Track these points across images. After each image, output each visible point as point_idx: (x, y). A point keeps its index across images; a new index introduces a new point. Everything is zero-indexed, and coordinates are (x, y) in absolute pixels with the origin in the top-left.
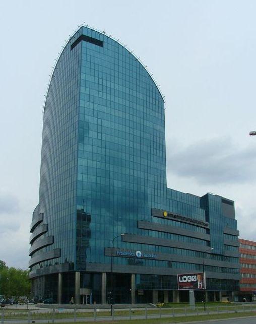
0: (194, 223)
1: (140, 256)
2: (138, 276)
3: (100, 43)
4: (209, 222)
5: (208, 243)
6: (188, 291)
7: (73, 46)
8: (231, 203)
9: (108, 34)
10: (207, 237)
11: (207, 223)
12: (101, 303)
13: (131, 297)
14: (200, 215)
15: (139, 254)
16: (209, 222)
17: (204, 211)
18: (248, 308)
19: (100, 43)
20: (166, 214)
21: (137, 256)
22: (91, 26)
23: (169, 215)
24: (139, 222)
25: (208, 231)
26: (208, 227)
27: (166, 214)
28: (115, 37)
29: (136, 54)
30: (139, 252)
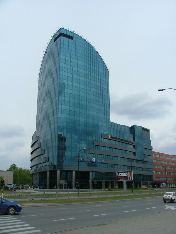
0: (126, 142)
1: (95, 161)
2: (94, 173)
3: (71, 38)
4: (135, 141)
5: (135, 154)
6: (123, 181)
7: (56, 39)
9: (76, 32)
10: (134, 150)
14: (129, 138)
15: (94, 160)
16: (135, 141)
18: (158, 191)
19: (71, 38)
20: (110, 137)
21: (93, 161)
22: (66, 28)
23: (111, 137)
25: (134, 147)
26: (134, 144)
27: (110, 137)
28: (80, 34)
29: (92, 44)
30: (94, 159)
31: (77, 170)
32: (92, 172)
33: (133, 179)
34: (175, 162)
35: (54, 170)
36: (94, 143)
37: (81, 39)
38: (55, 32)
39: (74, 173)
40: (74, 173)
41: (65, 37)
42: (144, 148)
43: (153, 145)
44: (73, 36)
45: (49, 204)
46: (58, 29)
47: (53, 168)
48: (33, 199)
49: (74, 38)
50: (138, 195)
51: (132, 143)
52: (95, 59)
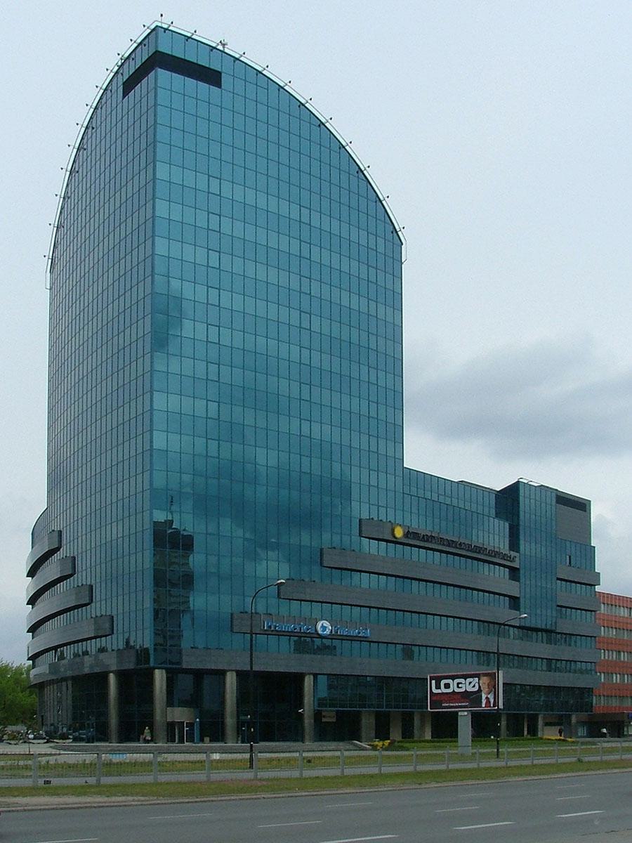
1: (327, 632)
3: (211, 77)
4: (518, 551)
5: (515, 602)
7: (129, 86)
9: (233, 49)
10: (513, 588)
12: (303, 741)
15: (324, 628)
17: (507, 525)
19: (211, 77)
21: (320, 632)
22: (184, 26)
25: (514, 573)
26: (516, 565)
27: (399, 533)
28: (255, 59)
30: (326, 624)
37: (262, 82)
42: (558, 579)
49: (225, 80)
51: (504, 557)
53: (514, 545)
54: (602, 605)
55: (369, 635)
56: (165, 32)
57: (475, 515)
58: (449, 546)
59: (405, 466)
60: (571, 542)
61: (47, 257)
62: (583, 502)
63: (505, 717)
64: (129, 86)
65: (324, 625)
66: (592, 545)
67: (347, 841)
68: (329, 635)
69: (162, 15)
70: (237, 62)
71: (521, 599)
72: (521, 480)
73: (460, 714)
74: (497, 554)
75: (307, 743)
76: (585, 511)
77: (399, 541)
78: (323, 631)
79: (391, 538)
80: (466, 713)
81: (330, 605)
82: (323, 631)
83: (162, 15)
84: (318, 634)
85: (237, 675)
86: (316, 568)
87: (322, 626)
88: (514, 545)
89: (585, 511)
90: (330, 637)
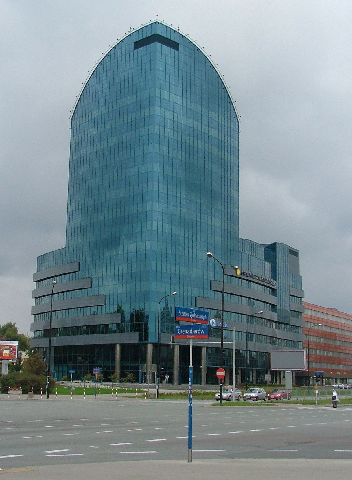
0: (262, 283)
1: (214, 325)
3: (174, 45)
4: (276, 280)
7: (138, 45)
8: (299, 251)
10: (273, 300)
11: (275, 282)
12: (201, 383)
13: (201, 377)
15: (213, 322)
19: (174, 45)
20: (239, 272)
21: (212, 325)
23: (242, 273)
24: (212, 282)
25: (274, 291)
27: (239, 272)
31: (157, 342)
32: (207, 348)
33: (273, 369)
34: (350, 330)
35: (140, 342)
36: (212, 285)
38: (138, 26)
39: (118, 348)
40: (118, 348)
41: (165, 44)
43: (304, 287)
44: (177, 41)
45: (205, 403)
46: (147, 22)
47: (138, 338)
48: (298, 399)
49: (180, 47)
50: (273, 398)
52: (187, 65)
53: (274, 275)
54: (305, 309)
55: (228, 327)
56: (158, 24)
57: (245, 254)
58: (255, 278)
59: (239, 237)
60: (248, 255)
61: (71, 112)
62: (296, 251)
63: (270, 372)
64: (138, 45)
65: (213, 321)
66: (300, 275)
67: (76, 455)
68: (215, 326)
69: (157, 16)
70: (176, 32)
71: (278, 307)
72: (276, 242)
73: (287, 372)
74: (264, 281)
75: (203, 385)
76: (297, 256)
77: (239, 277)
78: (213, 324)
79: (236, 276)
80: (289, 372)
81: (210, 310)
82: (213, 324)
83: (157, 16)
84: (211, 326)
85: (153, 345)
86: (209, 292)
87: (212, 321)
88: (274, 275)
89: (297, 256)
90: (215, 328)
